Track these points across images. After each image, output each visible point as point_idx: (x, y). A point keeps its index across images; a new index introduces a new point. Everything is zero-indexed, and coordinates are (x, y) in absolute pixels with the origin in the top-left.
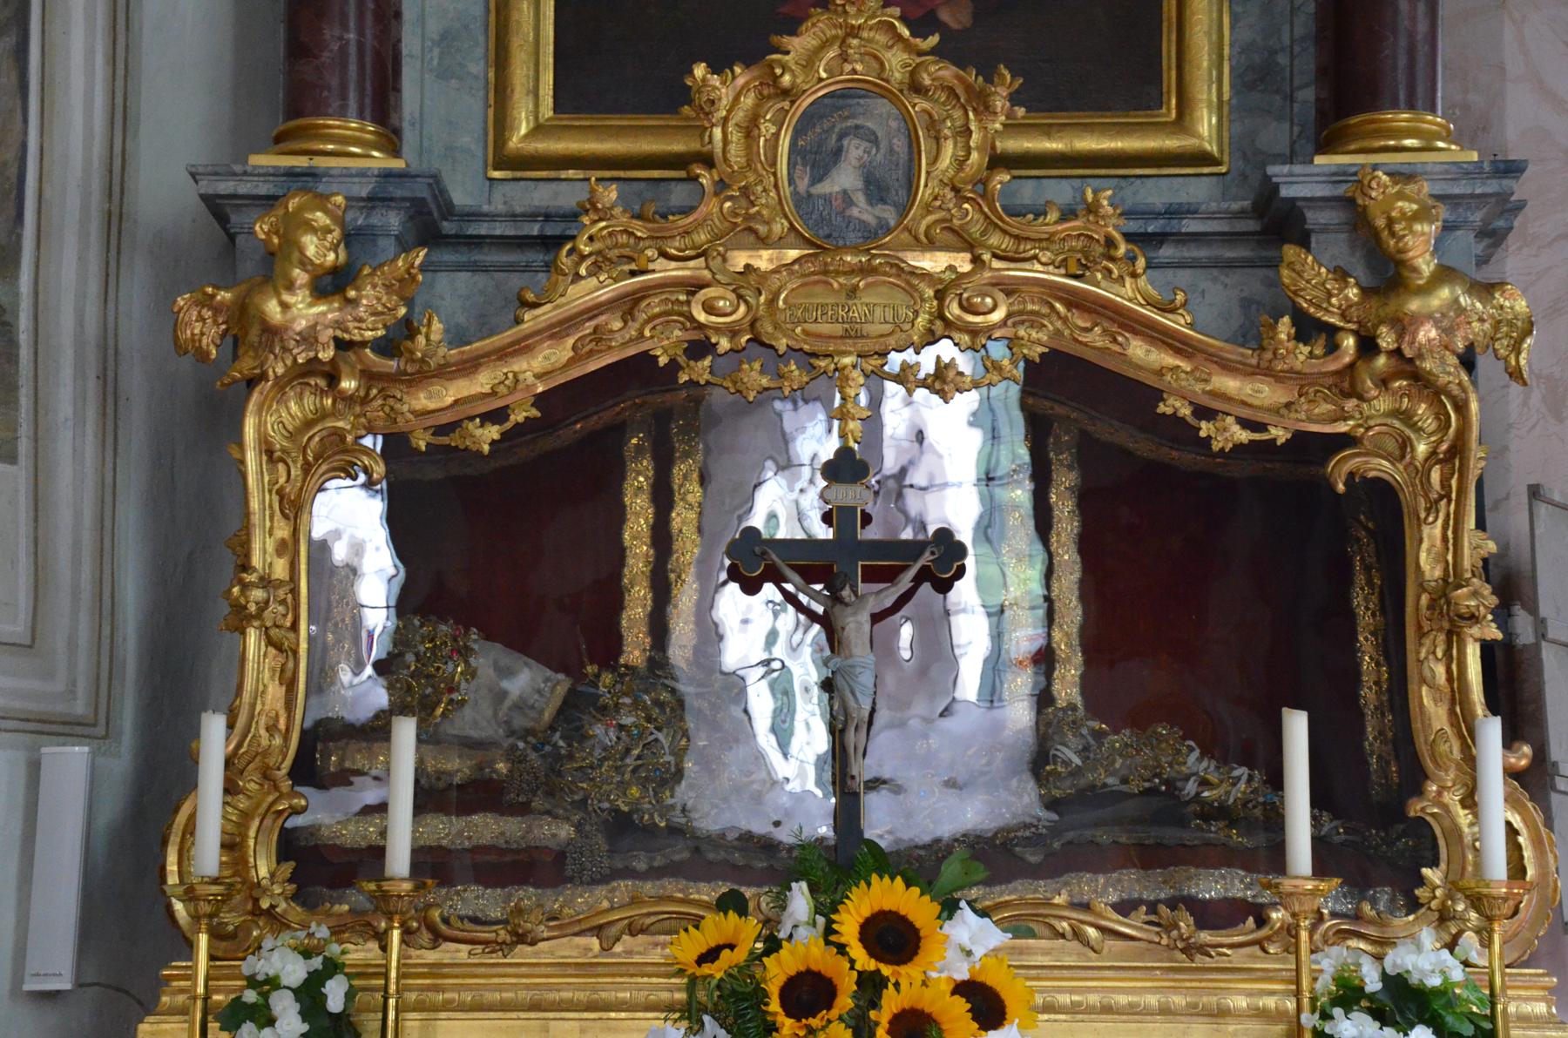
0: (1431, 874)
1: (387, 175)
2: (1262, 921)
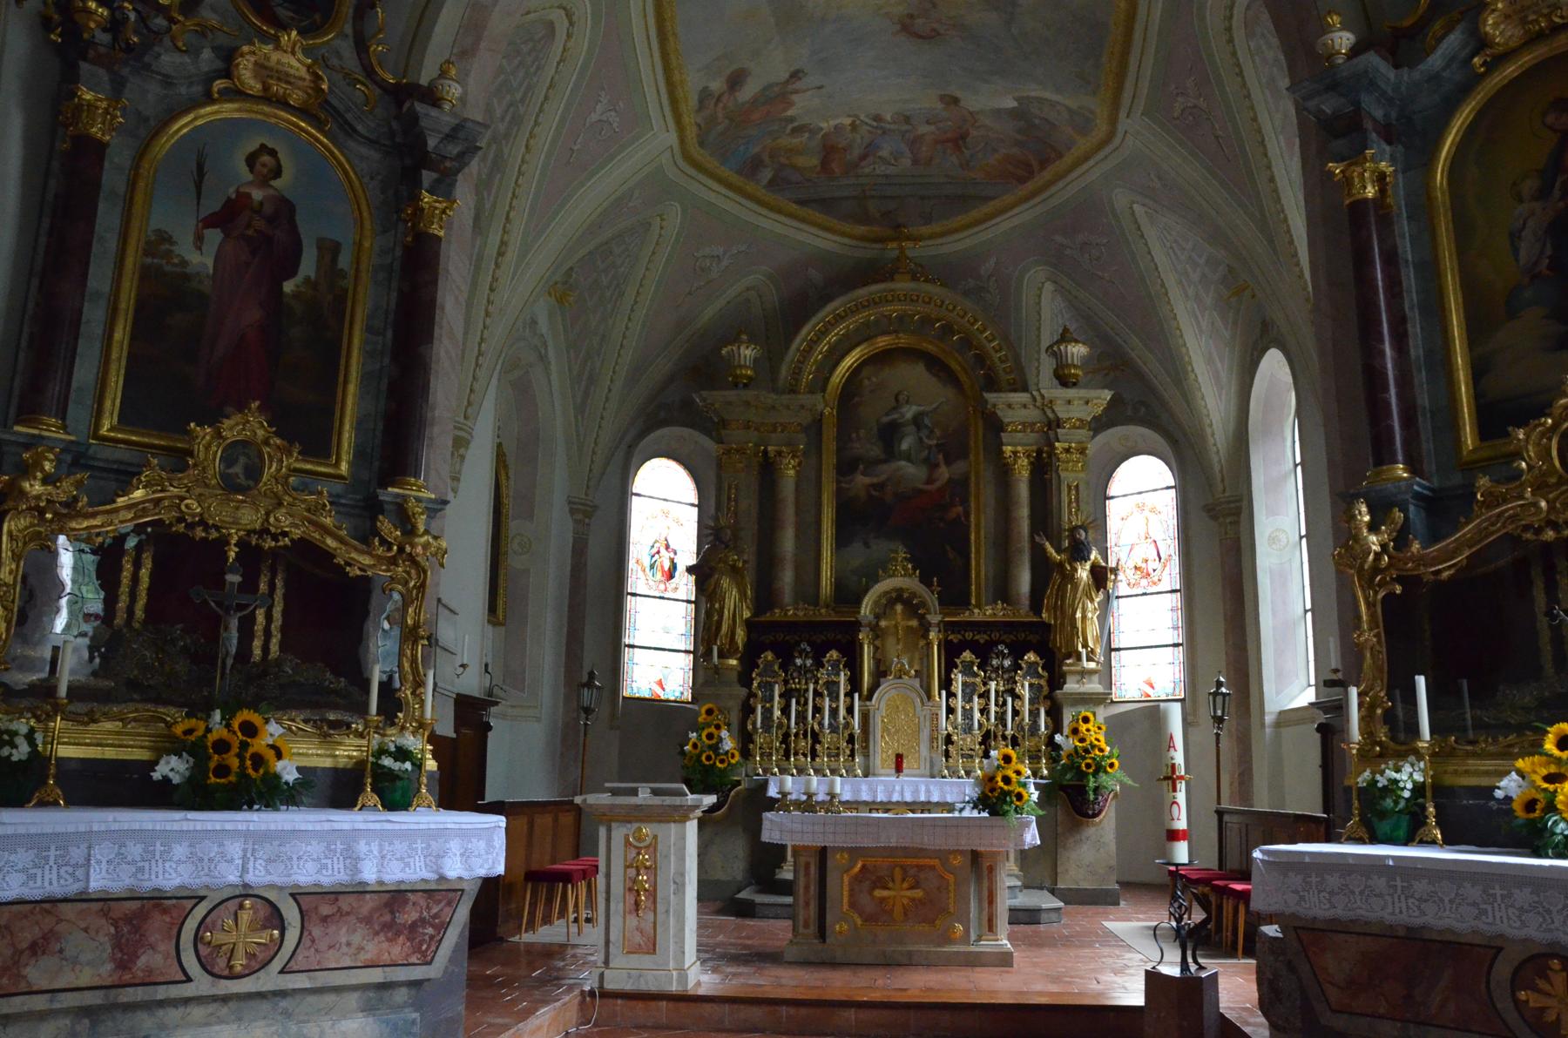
1: (72, 442)
2: (349, 727)
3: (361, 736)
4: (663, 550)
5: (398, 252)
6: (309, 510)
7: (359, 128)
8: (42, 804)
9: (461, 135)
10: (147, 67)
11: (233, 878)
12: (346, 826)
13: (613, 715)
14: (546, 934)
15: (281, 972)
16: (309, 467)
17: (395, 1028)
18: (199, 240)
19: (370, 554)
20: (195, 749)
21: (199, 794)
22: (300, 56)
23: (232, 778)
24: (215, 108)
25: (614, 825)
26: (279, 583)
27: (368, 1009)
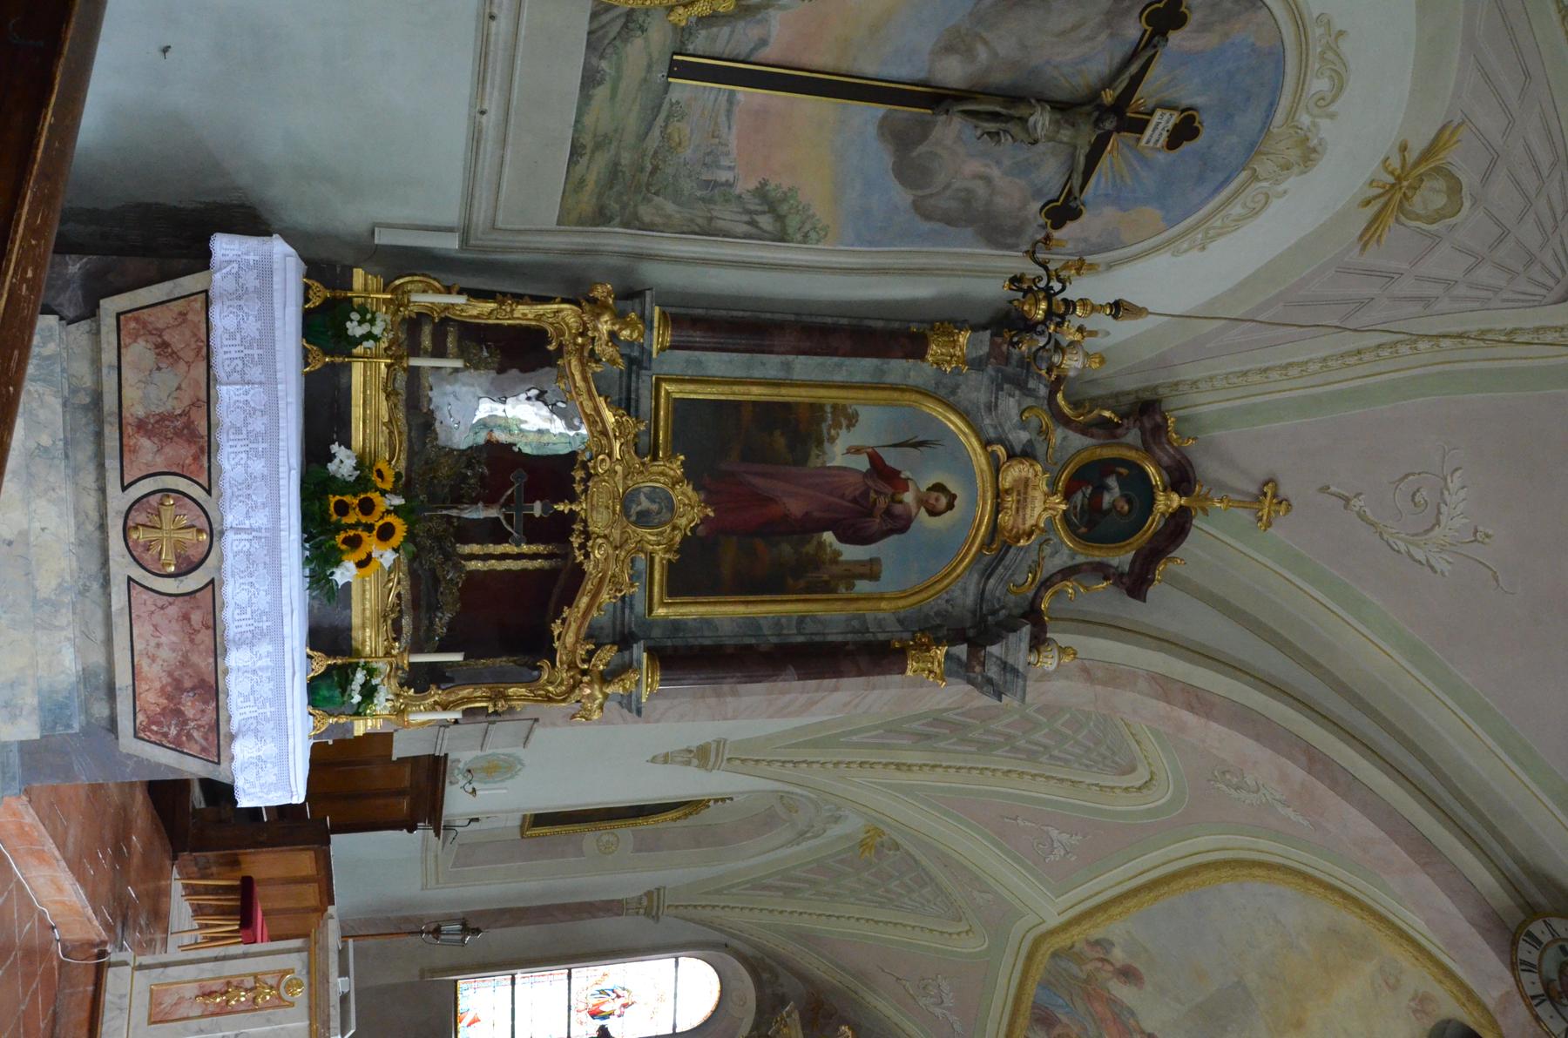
0: (412, 692)
1: (651, 354)
2: (395, 640)
3: (387, 654)
4: (622, 1001)
5: (881, 637)
6: (613, 576)
7: (992, 581)
8: (306, 354)
9: (1009, 677)
10: (1000, 388)
11: (230, 519)
12: (287, 630)
13: (435, 971)
14: (180, 909)
15: (130, 579)
16: (657, 576)
17: (62, 706)
18: (857, 451)
19: (577, 641)
20: (363, 481)
21: (316, 487)
22: (1045, 515)
23: (335, 517)
24: (979, 450)
25: (305, 954)
26: (538, 563)
27: (86, 676)
